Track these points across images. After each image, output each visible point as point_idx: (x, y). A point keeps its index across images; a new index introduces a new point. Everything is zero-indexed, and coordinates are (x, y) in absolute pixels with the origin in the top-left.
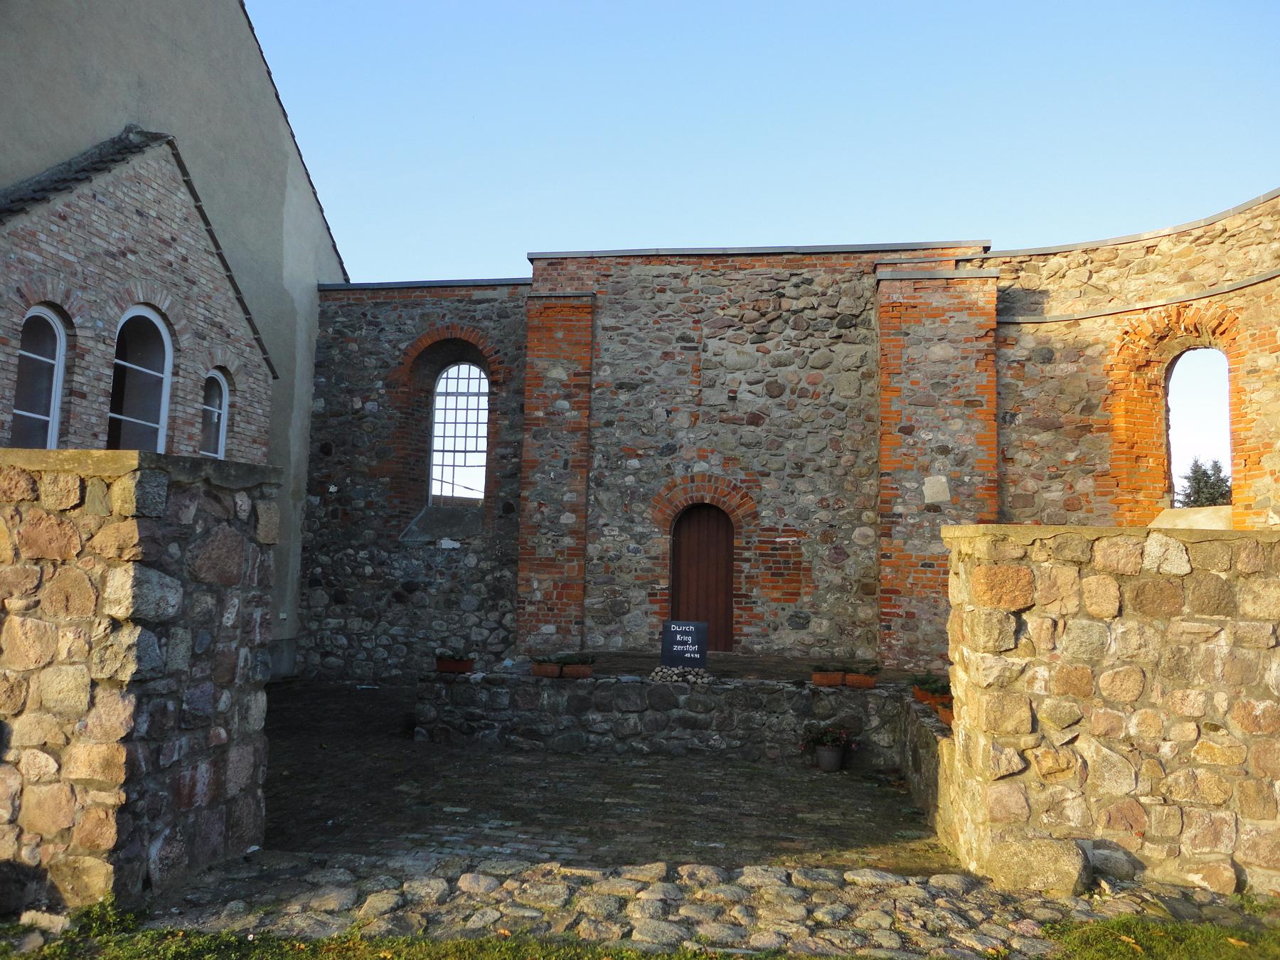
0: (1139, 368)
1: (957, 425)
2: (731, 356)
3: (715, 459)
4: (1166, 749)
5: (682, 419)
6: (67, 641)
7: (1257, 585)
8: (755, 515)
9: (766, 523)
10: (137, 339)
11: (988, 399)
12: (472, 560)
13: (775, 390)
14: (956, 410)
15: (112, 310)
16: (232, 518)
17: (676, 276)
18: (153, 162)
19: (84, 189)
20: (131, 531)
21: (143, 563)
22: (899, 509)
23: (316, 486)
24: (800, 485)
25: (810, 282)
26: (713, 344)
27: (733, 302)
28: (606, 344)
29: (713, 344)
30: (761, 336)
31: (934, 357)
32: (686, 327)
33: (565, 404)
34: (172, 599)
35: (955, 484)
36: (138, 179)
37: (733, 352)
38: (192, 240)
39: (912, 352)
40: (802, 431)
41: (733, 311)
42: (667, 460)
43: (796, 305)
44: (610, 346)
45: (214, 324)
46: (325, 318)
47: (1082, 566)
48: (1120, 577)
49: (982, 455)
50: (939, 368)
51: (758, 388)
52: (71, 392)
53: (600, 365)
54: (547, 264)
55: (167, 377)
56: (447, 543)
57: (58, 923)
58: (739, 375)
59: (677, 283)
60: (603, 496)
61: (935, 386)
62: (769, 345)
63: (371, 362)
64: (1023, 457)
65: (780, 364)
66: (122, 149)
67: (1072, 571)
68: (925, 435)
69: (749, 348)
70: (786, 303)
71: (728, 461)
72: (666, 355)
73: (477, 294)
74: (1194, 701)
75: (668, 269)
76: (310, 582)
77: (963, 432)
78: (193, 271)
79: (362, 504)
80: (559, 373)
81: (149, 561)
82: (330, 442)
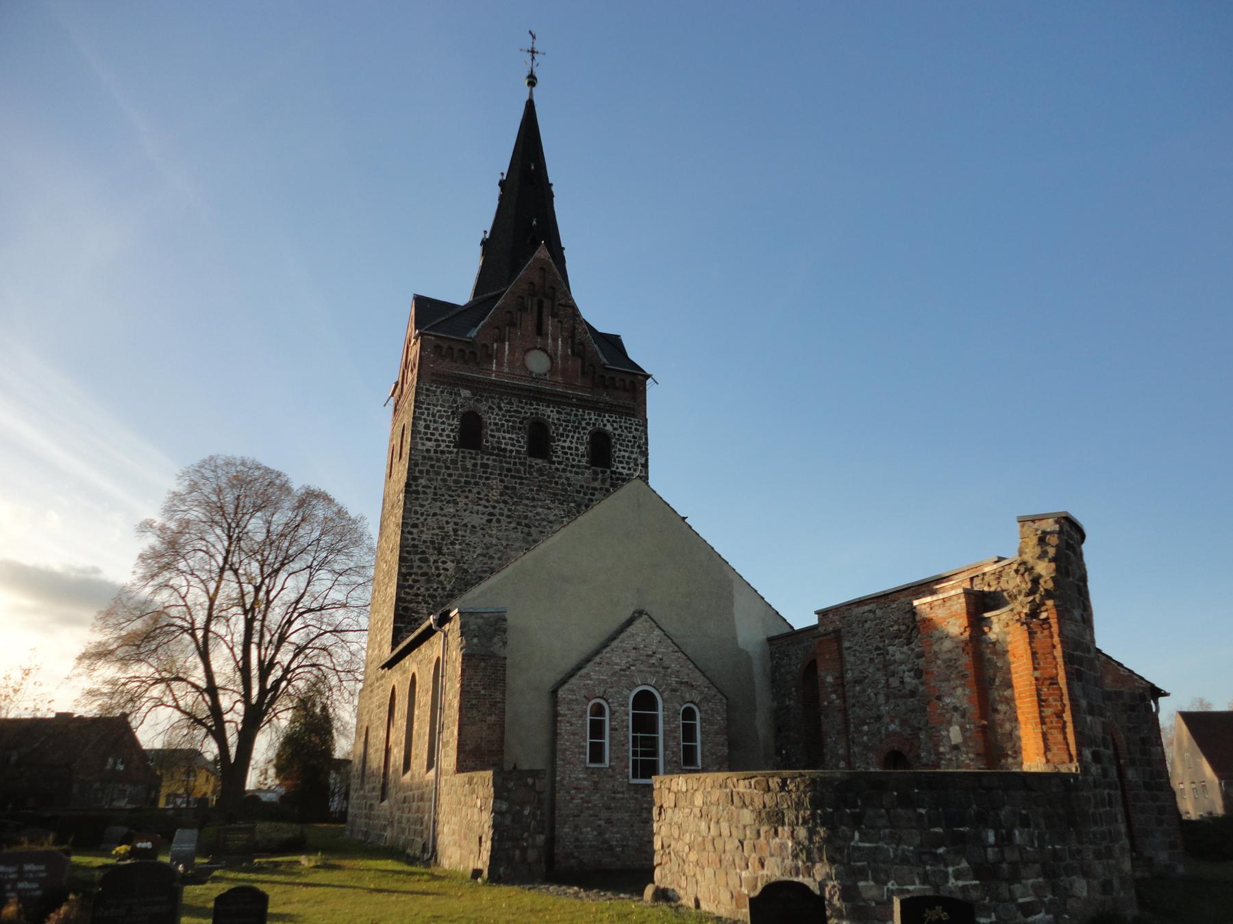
1: (959, 691)
5: (882, 699)
8: (918, 757)
10: (645, 701)
11: (970, 672)
14: (958, 682)
15: (626, 692)
16: (526, 785)
17: (870, 611)
19: (608, 649)
22: (942, 749)
26: (891, 649)
31: (944, 649)
32: (876, 642)
33: (834, 696)
34: (504, 807)
35: (963, 730)
39: (935, 648)
41: (896, 627)
45: (682, 683)
49: (973, 710)
50: (948, 656)
52: (612, 729)
54: (822, 614)
58: (903, 667)
59: (871, 616)
60: (856, 749)
62: (913, 646)
68: (948, 700)
69: (905, 649)
71: (903, 723)
72: (872, 660)
75: (867, 608)
78: (666, 662)
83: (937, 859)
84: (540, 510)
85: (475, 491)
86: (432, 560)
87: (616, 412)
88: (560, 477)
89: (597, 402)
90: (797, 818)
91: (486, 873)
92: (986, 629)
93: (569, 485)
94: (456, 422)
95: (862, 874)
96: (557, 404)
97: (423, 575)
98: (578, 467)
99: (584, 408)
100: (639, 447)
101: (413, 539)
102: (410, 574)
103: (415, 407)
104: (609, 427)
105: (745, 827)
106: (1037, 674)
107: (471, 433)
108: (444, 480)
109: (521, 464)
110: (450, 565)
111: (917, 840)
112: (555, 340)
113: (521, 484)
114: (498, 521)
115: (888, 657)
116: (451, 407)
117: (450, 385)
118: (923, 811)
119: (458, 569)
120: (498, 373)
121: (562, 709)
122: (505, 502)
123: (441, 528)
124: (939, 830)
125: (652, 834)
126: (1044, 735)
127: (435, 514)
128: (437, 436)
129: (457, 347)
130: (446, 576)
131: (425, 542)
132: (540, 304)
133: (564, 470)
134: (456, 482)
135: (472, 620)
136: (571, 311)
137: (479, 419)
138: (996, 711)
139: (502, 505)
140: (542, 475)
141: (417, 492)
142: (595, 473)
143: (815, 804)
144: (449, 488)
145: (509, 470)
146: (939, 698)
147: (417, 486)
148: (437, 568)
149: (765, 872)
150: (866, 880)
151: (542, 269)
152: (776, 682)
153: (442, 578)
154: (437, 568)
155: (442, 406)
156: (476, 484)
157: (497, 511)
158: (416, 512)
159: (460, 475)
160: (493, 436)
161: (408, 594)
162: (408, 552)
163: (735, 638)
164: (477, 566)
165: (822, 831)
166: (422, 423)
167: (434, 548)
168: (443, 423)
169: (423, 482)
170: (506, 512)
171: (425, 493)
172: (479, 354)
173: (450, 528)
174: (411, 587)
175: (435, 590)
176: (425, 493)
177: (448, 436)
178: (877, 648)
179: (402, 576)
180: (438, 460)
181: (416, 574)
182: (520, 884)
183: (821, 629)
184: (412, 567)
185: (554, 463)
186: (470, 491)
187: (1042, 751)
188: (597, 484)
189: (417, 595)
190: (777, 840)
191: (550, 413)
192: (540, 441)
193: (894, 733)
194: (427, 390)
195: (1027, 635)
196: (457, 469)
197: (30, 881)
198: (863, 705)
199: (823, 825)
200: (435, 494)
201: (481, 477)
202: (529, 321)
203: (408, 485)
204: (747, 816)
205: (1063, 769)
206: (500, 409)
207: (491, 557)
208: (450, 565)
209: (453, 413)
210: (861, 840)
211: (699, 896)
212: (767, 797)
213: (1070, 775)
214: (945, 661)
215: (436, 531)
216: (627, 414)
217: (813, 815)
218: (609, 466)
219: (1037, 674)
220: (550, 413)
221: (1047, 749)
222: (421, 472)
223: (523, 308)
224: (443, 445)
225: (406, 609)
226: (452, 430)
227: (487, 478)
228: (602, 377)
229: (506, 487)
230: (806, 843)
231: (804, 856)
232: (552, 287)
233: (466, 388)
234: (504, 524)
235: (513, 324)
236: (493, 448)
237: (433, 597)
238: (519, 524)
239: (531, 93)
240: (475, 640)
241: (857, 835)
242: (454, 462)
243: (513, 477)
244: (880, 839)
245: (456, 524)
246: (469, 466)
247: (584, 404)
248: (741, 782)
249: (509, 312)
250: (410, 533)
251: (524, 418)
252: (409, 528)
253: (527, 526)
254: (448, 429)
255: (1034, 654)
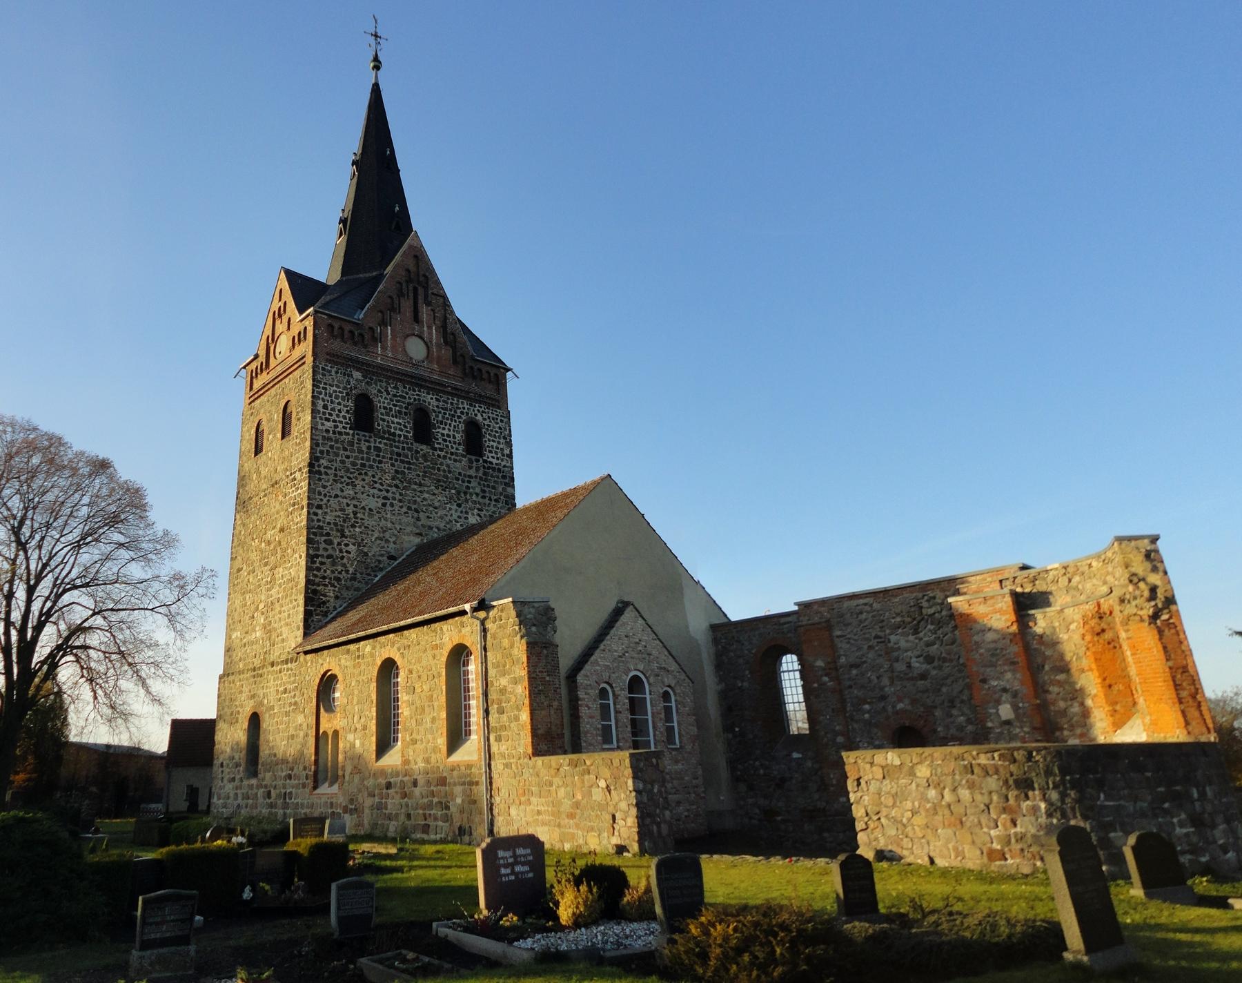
0: (1098, 634)
1: (1009, 675)
2: (903, 644)
3: (907, 701)
4: (905, 820)
5: (885, 681)
6: (623, 796)
7: (919, 766)
8: (935, 731)
9: (942, 734)
10: (635, 684)
11: (1021, 660)
12: (809, 764)
13: (929, 659)
14: (1006, 668)
18: (628, 615)
20: (630, 770)
21: (634, 778)
22: (990, 724)
23: (728, 728)
24: (955, 712)
25: (934, 598)
26: (893, 638)
27: (898, 614)
28: (840, 645)
29: (893, 638)
30: (916, 632)
32: (876, 631)
33: (826, 679)
34: (641, 786)
35: (1015, 708)
36: (624, 624)
37: (900, 640)
38: (647, 637)
39: (976, 638)
40: (949, 681)
41: (899, 619)
42: (883, 704)
43: (931, 611)
44: (843, 646)
46: (716, 641)
47: (872, 764)
48: (883, 767)
49: (1026, 690)
50: (992, 646)
51: (921, 659)
52: (617, 712)
53: (839, 657)
55: (648, 696)
56: (795, 755)
57: (630, 855)
58: (909, 653)
59: (868, 608)
60: (856, 726)
61: (993, 655)
62: (921, 635)
63: (741, 661)
64: (1054, 689)
65: (929, 644)
66: (618, 613)
67: (868, 766)
69: (911, 638)
70: (924, 611)
71: (914, 702)
72: (870, 647)
73: (783, 620)
74: (909, 805)
75: (862, 601)
76: (736, 780)
77: (1012, 679)
79: (751, 736)
80: (820, 663)
81: (635, 777)
82: (730, 704)
83: (1166, 812)
84: (426, 495)
85: (370, 474)
86: (336, 541)
87: (485, 403)
88: (442, 464)
89: (468, 392)
90: (1047, 783)
91: (635, 847)
92: (1031, 624)
93: (450, 472)
94: (351, 404)
95: (1111, 827)
96: (438, 392)
97: (329, 557)
98: (457, 454)
99: (459, 397)
100: (505, 438)
101: (319, 521)
102: (317, 556)
103: (314, 385)
104: (479, 418)
105: (990, 793)
106: (1170, 663)
107: (364, 416)
108: (343, 462)
109: (409, 449)
110: (352, 548)
111: (1149, 798)
112: (430, 327)
113: (409, 469)
114: (392, 505)
115: (891, 645)
116: (345, 388)
117: (343, 365)
118: (1149, 774)
119: (360, 552)
120: (384, 356)
121: (581, 694)
122: (396, 486)
123: (343, 510)
124: (1161, 789)
125: (849, 806)
126: (1183, 712)
127: (336, 496)
128: (334, 417)
129: (347, 328)
130: (349, 559)
131: (329, 523)
132: (415, 290)
133: (445, 457)
134: (354, 464)
135: (526, 610)
136: (442, 300)
137: (370, 402)
138: (1047, 692)
139: (394, 489)
140: (426, 461)
141: (320, 473)
142: (470, 461)
143: (1063, 772)
144: (348, 470)
145: (399, 455)
146: (984, 681)
147: (319, 466)
148: (341, 551)
149: (1018, 829)
150: (1115, 831)
151: (416, 257)
152: (720, 665)
153: (345, 561)
154: (341, 551)
155: (338, 386)
156: (371, 467)
157: (390, 495)
158: (320, 494)
159: (356, 458)
160: (383, 420)
161: (316, 576)
162: (315, 534)
163: (687, 627)
164: (375, 550)
165: (1072, 793)
166: (321, 402)
167: (337, 530)
168: (339, 404)
169: (324, 462)
170: (397, 496)
171: (326, 474)
172: (365, 337)
173: (350, 510)
174: (318, 569)
175: (340, 573)
176: (326, 474)
177: (345, 417)
178: (877, 637)
179: (311, 558)
180: (337, 441)
181: (322, 556)
182: (786, 855)
183: (804, 620)
184: (318, 549)
185: (436, 449)
186: (366, 474)
187: (1183, 724)
188: (472, 472)
189: (324, 578)
190: (1028, 802)
191: (430, 400)
192: (423, 428)
193: (903, 711)
194: (323, 369)
195: (1156, 632)
196: (353, 451)
197: (523, 864)
198: (863, 687)
199: (1072, 789)
200: (336, 475)
201: (374, 461)
202: (407, 305)
203: (311, 465)
204: (993, 783)
205: (1203, 739)
206: (388, 393)
207: (387, 541)
208: (352, 548)
209: (348, 394)
210: (1106, 799)
211: (932, 854)
212: (1013, 768)
213: (1209, 744)
214: (988, 650)
215: (339, 513)
216: (493, 406)
217: (1063, 781)
218: (481, 455)
219: (1170, 663)
220: (430, 400)
221: (1187, 723)
222: (322, 452)
223: (401, 294)
224: (340, 426)
225: (315, 592)
226: (348, 412)
227: (380, 462)
228: (471, 368)
229: (397, 472)
230: (1059, 804)
231: (1058, 814)
232: (424, 276)
233: (358, 370)
234: (397, 508)
235: (392, 309)
236: (384, 432)
237: (338, 580)
238: (409, 508)
239: (376, 77)
240: (534, 629)
241: (1102, 796)
242: (351, 444)
243: (402, 462)
244: (1120, 799)
245: (355, 506)
246: (364, 449)
247: (457, 393)
248: (982, 756)
249: (390, 297)
250: (316, 514)
251: (409, 404)
252: (314, 510)
253: (416, 511)
254: (344, 410)
255: (1165, 648)
